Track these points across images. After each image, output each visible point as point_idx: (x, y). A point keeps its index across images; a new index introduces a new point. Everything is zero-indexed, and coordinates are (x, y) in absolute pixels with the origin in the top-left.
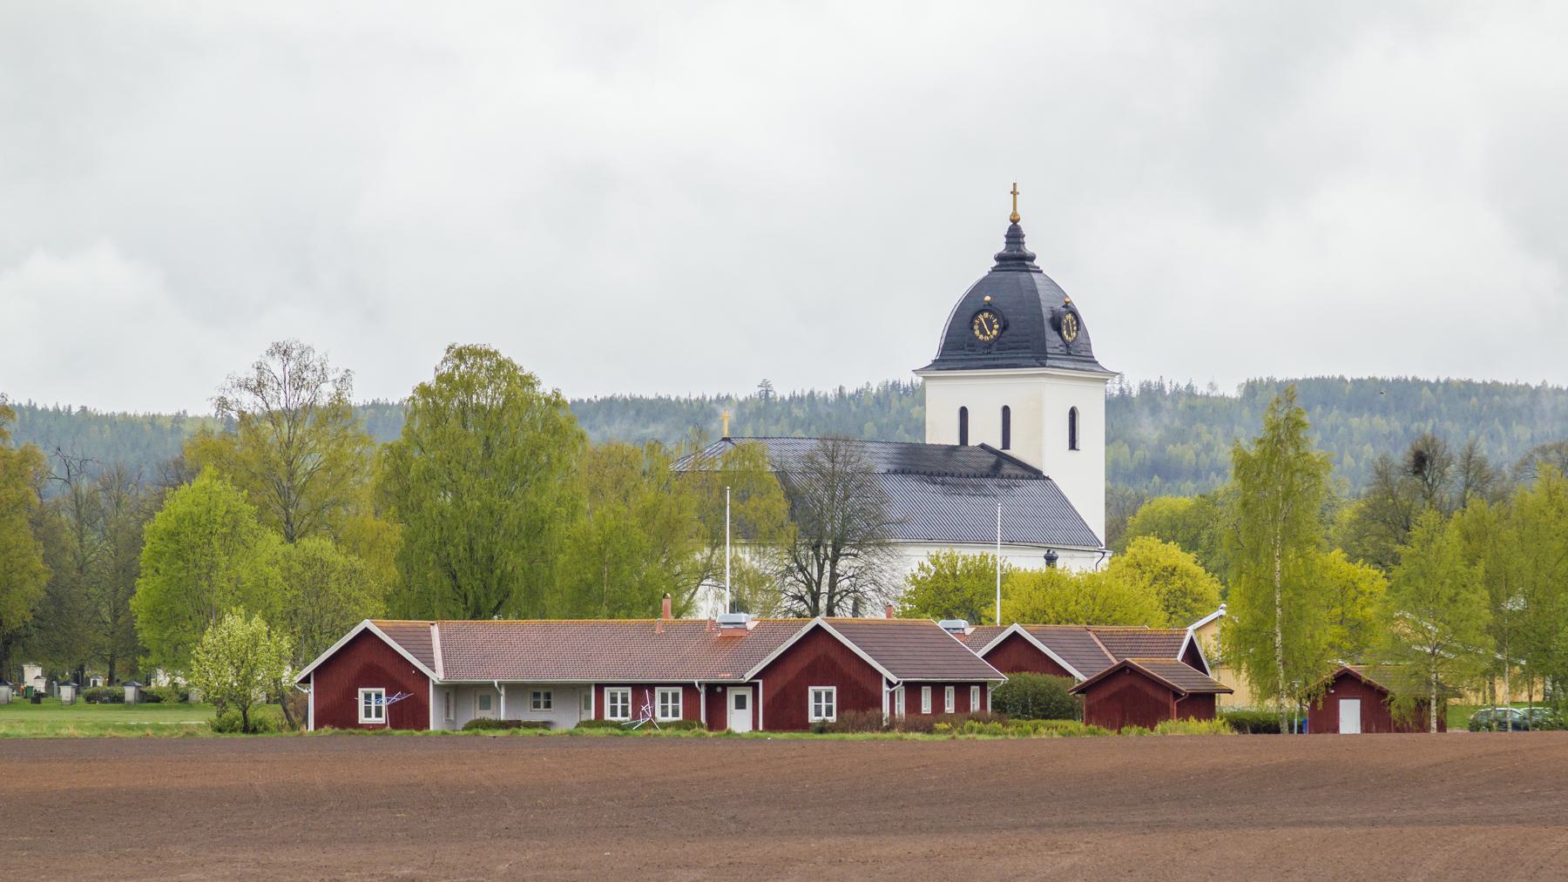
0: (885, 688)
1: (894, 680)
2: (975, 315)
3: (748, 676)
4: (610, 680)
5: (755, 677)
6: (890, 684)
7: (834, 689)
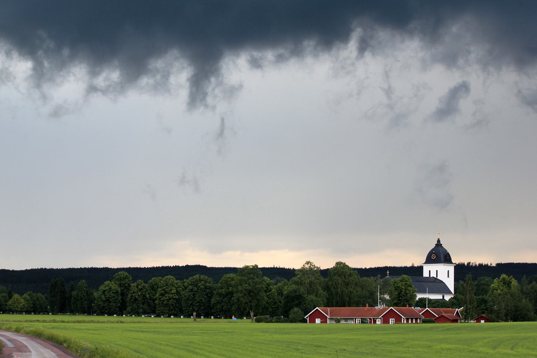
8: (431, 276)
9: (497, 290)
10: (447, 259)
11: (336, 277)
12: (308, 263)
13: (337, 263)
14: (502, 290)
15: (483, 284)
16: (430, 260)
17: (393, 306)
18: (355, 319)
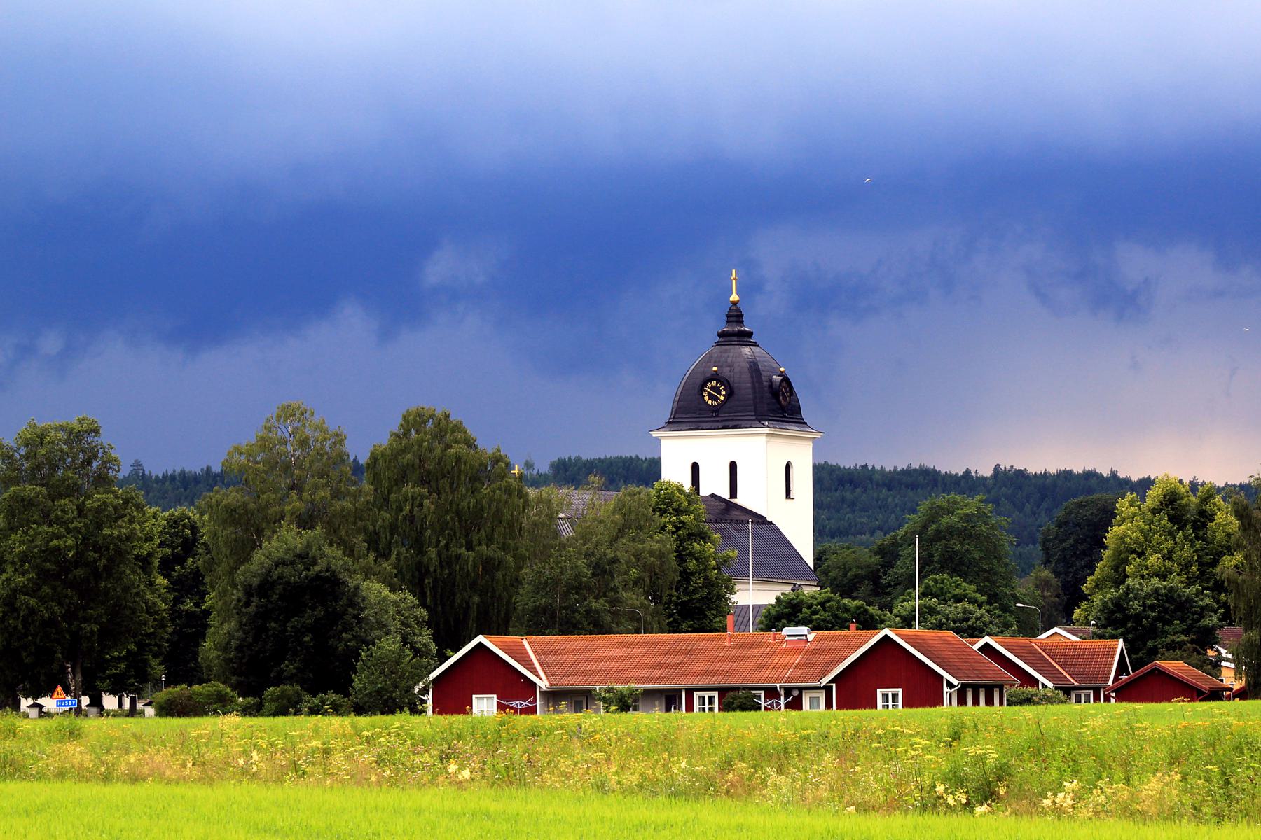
0: (946, 689)
1: (955, 682)
2: (704, 384)
3: (824, 682)
4: (700, 685)
5: (831, 682)
6: (950, 685)
7: (900, 691)
8: (705, 491)
9: (1141, 554)
10: (774, 405)
11: (409, 489)
12: (288, 413)
13: (415, 421)
14: (1168, 556)
15: (951, 532)
16: (693, 413)
17: (487, 632)
18: (690, 692)
